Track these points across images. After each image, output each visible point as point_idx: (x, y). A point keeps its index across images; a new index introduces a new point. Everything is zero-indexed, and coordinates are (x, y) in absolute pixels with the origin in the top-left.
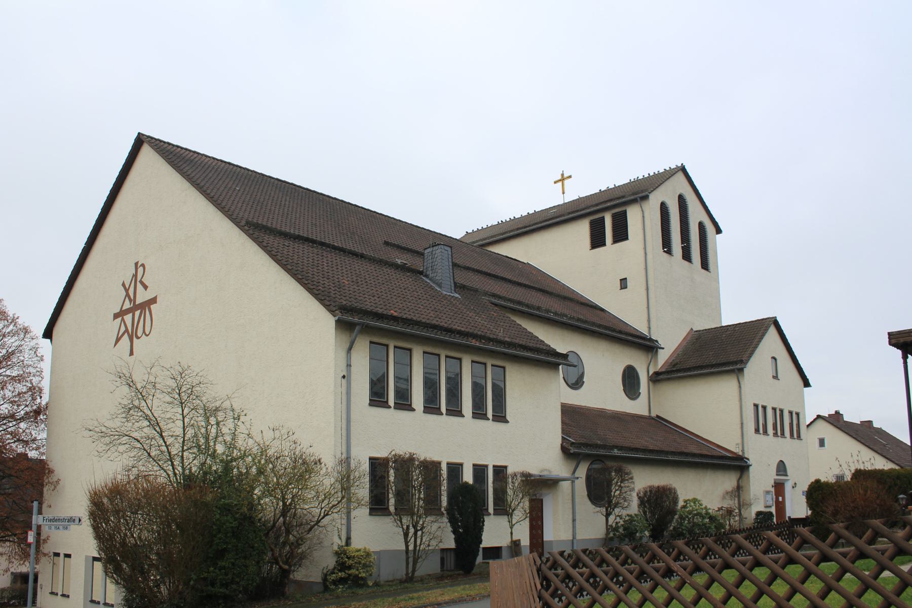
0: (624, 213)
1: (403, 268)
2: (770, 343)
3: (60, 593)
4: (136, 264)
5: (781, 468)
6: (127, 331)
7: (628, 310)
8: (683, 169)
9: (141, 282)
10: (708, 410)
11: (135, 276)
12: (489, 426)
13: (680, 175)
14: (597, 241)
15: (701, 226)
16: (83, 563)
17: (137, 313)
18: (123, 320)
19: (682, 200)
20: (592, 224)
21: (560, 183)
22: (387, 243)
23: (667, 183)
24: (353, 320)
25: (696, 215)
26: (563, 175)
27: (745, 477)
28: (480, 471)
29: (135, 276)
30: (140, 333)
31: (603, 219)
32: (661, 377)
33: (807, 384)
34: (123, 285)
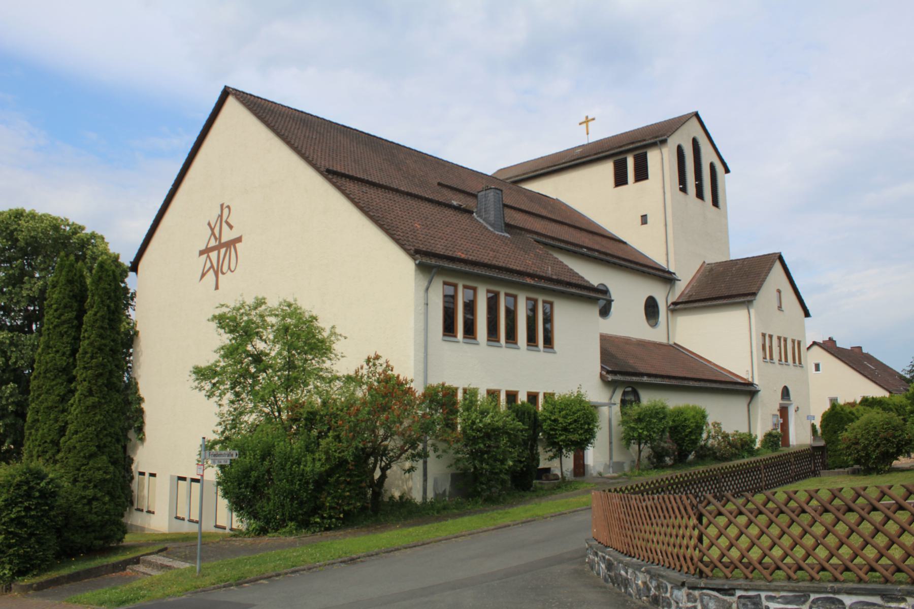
0: (645, 155)
1: (458, 209)
3: (145, 510)
4: (222, 206)
5: (786, 393)
6: (212, 267)
7: (649, 244)
8: (697, 115)
9: (227, 223)
10: (720, 339)
11: (221, 216)
12: (540, 356)
13: (694, 120)
14: (620, 179)
15: (712, 166)
16: (168, 482)
17: (223, 251)
18: (208, 256)
19: (695, 143)
21: (584, 125)
22: (439, 184)
23: (684, 127)
24: (430, 262)
25: (708, 156)
26: (587, 117)
27: (753, 402)
29: (221, 216)
30: (225, 269)
31: (625, 160)
32: (678, 306)
33: (807, 314)
34: (209, 224)
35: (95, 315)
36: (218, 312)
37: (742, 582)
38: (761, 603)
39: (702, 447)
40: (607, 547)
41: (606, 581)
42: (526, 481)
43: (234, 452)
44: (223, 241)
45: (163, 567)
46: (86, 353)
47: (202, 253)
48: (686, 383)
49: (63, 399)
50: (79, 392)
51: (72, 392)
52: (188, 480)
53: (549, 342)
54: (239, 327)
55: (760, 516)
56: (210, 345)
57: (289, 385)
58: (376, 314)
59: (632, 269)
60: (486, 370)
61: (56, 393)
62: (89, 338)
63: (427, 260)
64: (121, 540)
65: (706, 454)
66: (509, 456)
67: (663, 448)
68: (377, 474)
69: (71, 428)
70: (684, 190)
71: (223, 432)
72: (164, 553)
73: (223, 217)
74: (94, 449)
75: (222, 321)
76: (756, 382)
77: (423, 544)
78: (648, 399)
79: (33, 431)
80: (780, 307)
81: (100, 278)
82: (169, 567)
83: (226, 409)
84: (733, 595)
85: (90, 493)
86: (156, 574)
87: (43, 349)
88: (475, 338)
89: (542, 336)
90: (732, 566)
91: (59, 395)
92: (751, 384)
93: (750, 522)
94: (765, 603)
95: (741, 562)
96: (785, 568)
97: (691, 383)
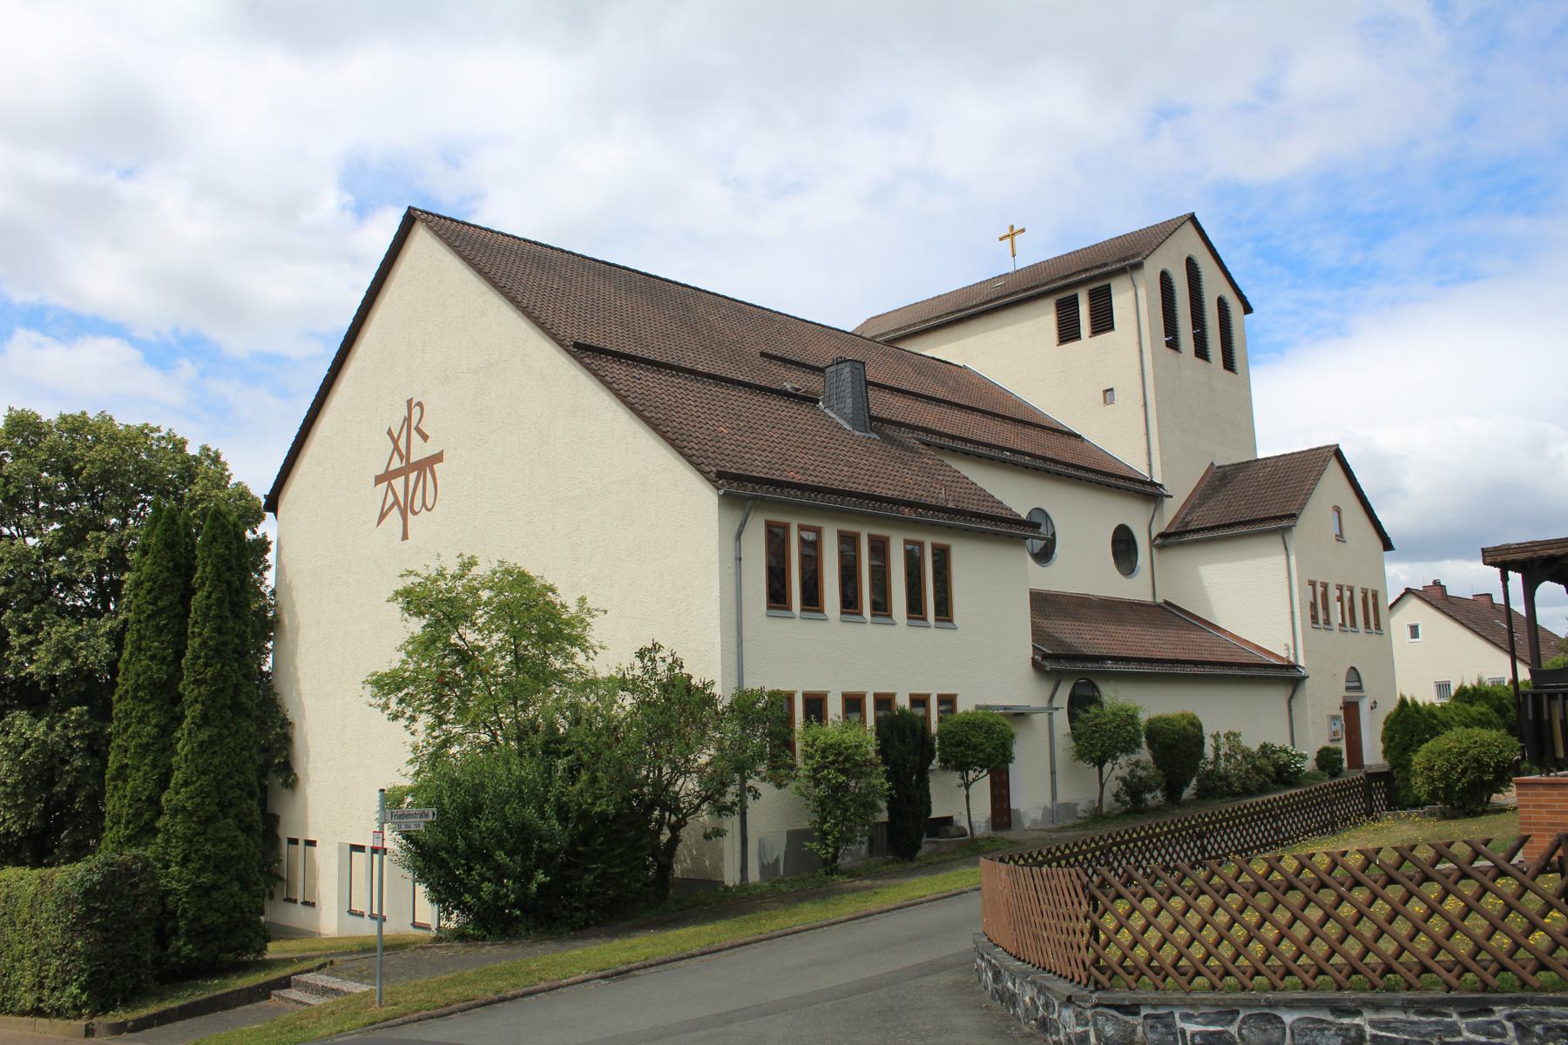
2: (1331, 483)
3: (300, 900)
4: (409, 402)
6: (396, 502)
7: (1120, 438)
8: (1192, 219)
10: (1247, 595)
11: (408, 419)
12: (930, 635)
13: (1189, 226)
14: (1068, 332)
15: (1222, 304)
17: (413, 476)
18: (390, 485)
19: (1191, 265)
20: (1060, 306)
22: (763, 354)
24: (740, 489)
25: (1213, 287)
26: (1012, 228)
28: (919, 701)
29: (408, 419)
30: (417, 505)
31: (1075, 298)
32: (1170, 540)
34: (390, 433)
35: (209, 597)
36: (400, 585)
37: (1152, 995)
38: (1173, 1025)
39: (1208, 775)
40: (997, 946)
41: (993, 998)
42: (910, 837)
43: (430, 811)
44: (413, 460)
45: (325, 991)
46: (198, 657)
47: (379, 480)
48: (1178, 670)
49: (165, 731)
50: (189, 720)
51: (179, 719)
52: (368, 850)
53: (944, 611)
54: (437, 607)
55: (1259, 895)
56: (391, 638)
57: (515, 694)
58: (652, 575)
59: (1089, 481)
60: (848, 660)
61: (154, 721)
62: (200, 634)
63: (735, 488)
64: (261, 951)
65: (1215, 787)
66: (892, 792)
67: (1140, 778)
68: (665, 836)
69: (178, 776)
70: (1173, 344)
71: (417, 774)
72: (325, 970)
73: (412, 421)
74: (215, 808)
75: (412, 600)
76: (1301, 662)
77: (733, 947)
78: (1115, 696)
79: (120, 783)
80: (1340, 537)
81: (214, 539)
82: (337, 992)
83: (420, 738)
84: (1137, 1014)
85: (205, 879)
86: (316, 1001)
87: (131, 654)
88: (821, 611)
89: (933, 600)
90: (1137, 972)
91: (156, 726)
92: (1294, 667)
93: (1341, 900)
94: (1180, 1024)
95: (1121, 965)
96: (1402, 970)
97: (1188, 670)
